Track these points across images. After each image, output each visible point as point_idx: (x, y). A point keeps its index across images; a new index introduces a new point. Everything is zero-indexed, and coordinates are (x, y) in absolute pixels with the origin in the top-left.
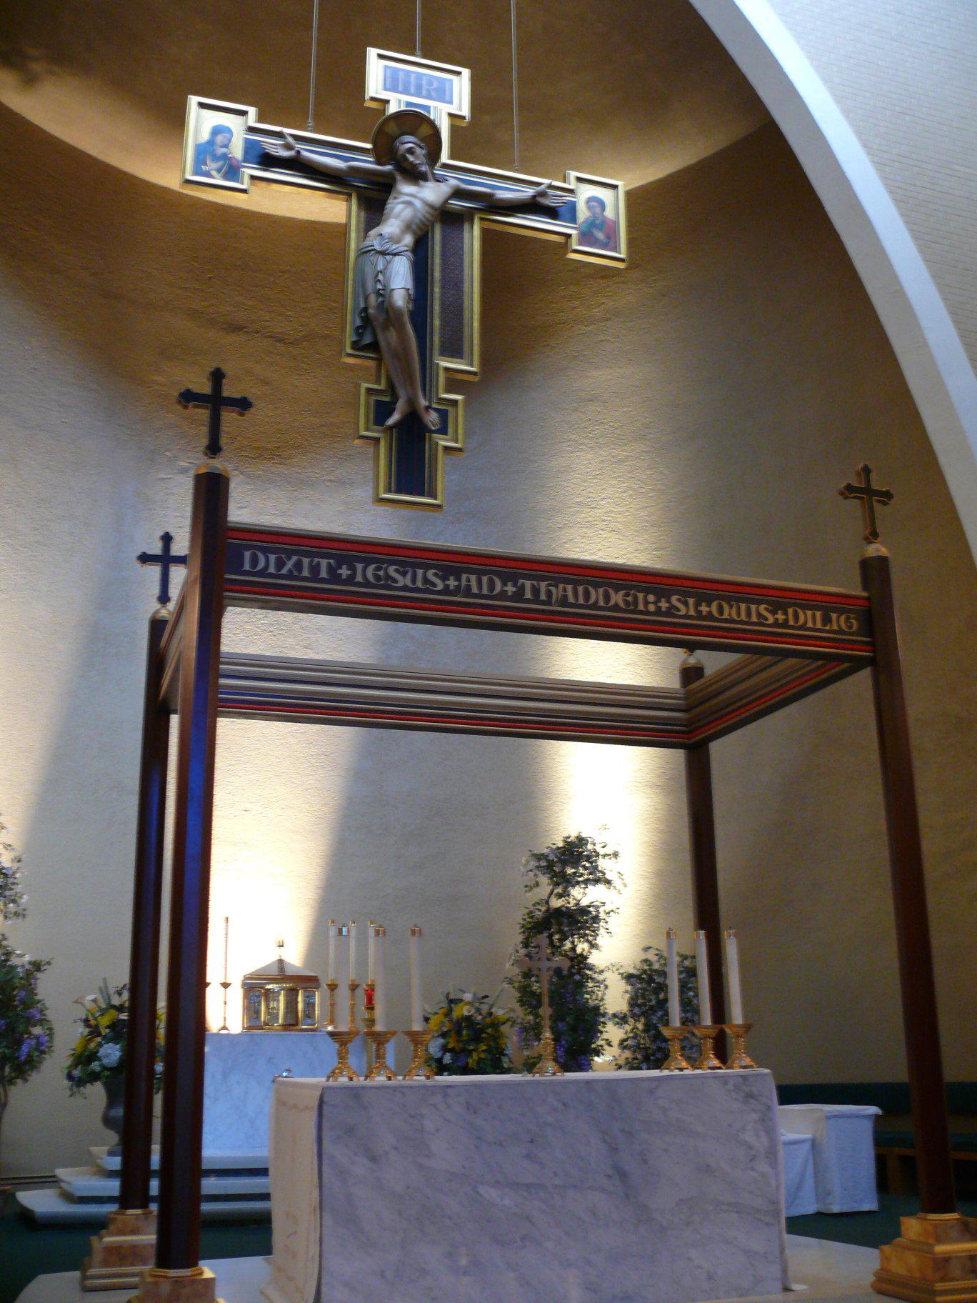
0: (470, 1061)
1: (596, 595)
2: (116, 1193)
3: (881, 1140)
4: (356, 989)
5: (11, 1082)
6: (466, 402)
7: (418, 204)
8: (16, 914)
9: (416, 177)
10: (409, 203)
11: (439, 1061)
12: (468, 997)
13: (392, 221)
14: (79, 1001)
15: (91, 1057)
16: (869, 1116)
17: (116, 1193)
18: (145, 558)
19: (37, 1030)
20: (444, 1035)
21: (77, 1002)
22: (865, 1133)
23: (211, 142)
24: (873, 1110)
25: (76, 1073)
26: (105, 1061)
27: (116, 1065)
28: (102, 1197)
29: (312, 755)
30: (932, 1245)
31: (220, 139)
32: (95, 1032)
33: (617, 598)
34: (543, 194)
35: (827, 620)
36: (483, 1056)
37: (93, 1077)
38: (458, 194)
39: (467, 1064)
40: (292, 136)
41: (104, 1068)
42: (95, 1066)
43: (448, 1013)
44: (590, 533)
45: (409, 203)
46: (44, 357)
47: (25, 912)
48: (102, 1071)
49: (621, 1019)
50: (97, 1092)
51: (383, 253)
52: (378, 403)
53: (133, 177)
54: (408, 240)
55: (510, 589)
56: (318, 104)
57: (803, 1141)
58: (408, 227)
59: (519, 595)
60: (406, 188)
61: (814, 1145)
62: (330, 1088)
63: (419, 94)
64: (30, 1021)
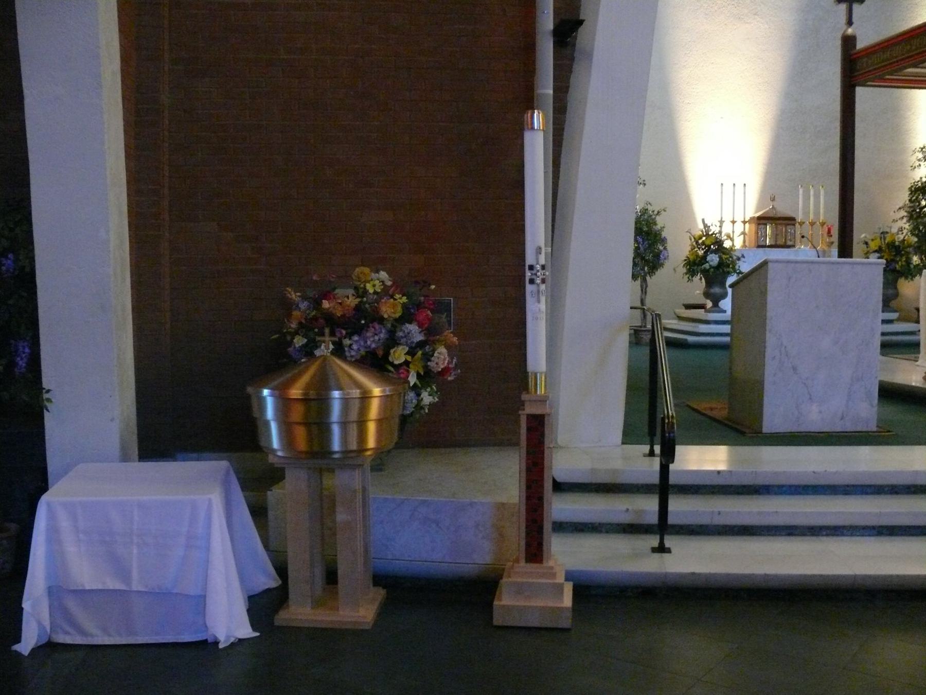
0: (897, 267)
2: (729, 331)
4: (814, 224)
14: (689, 231)
15: (704, 259)
17: (729, 331)
21: (687, 232)
26: (711, 263)
27: (716, 265)
28: (714, 333)
29: (760, 83)
36: (904, 263)
39: (896, 268)
41: (711, 267)
46: (333, 208)
47: (645, 182)
48: (710, 268)
49: (19, 361)
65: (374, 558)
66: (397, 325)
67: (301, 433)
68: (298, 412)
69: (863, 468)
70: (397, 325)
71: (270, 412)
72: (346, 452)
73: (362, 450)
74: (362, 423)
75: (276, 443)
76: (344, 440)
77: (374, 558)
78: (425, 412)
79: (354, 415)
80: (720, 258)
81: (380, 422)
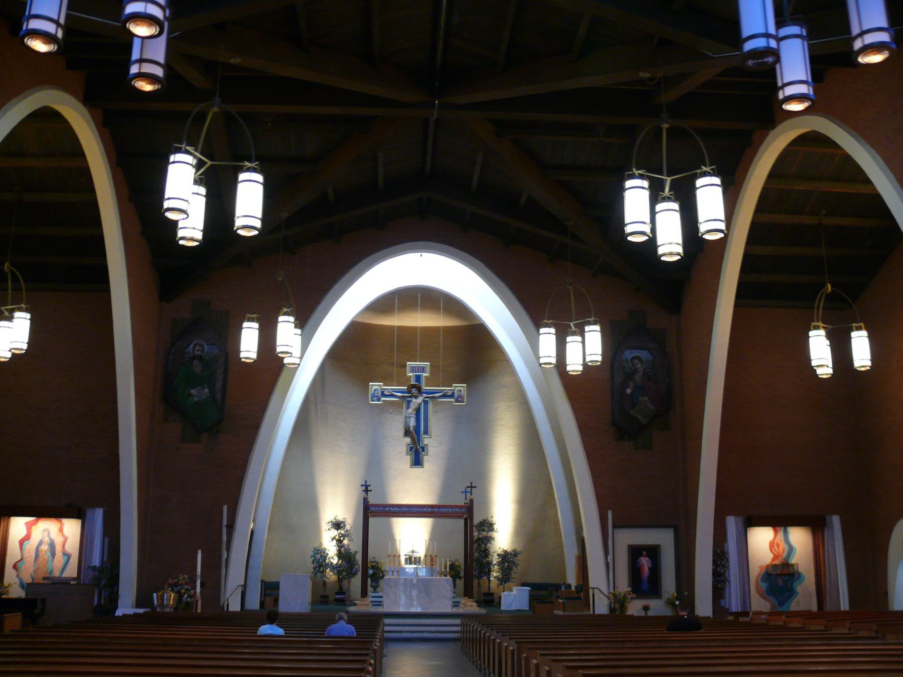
1: (422, 509)
3: (530, 596)
5: (352, 578)
6: (467, 386)
8: (351, 540)
9: (416, 397)
10: (414, 404)
13: (411, 408)
16: (528, 590)
19: (356, 566)
22: (707, 615)
24: (529, 588)
30: (333, 567)
31: (376, 392)
34: (446, 393)
35: (461, 510)
38: (426, 397)
40: (391, 389)
44: (503, 428)
45: (414, 404)
51: (409, 417)
52: (410, 447)
53: (372, 324)
54: (415, 412)
55: (408, 509)
56: (421, 303)
59: (410, 510)
60: (414, 400)
63: (418, 372)
65: (466, 499)
66: (495, 560)
67: (160, 601)
68: (159, 597)
69: (763, 159)
70: (495, 560)
71: (155, 597)
72: (167, 604)
73: (169, 604)
74: (170, 600)
75: (155, 602)
76: (167, 602)
77: (466, 499)
78: (342, 561)
79: (168, 598)
80: (374, 571)
81: (173, 600)
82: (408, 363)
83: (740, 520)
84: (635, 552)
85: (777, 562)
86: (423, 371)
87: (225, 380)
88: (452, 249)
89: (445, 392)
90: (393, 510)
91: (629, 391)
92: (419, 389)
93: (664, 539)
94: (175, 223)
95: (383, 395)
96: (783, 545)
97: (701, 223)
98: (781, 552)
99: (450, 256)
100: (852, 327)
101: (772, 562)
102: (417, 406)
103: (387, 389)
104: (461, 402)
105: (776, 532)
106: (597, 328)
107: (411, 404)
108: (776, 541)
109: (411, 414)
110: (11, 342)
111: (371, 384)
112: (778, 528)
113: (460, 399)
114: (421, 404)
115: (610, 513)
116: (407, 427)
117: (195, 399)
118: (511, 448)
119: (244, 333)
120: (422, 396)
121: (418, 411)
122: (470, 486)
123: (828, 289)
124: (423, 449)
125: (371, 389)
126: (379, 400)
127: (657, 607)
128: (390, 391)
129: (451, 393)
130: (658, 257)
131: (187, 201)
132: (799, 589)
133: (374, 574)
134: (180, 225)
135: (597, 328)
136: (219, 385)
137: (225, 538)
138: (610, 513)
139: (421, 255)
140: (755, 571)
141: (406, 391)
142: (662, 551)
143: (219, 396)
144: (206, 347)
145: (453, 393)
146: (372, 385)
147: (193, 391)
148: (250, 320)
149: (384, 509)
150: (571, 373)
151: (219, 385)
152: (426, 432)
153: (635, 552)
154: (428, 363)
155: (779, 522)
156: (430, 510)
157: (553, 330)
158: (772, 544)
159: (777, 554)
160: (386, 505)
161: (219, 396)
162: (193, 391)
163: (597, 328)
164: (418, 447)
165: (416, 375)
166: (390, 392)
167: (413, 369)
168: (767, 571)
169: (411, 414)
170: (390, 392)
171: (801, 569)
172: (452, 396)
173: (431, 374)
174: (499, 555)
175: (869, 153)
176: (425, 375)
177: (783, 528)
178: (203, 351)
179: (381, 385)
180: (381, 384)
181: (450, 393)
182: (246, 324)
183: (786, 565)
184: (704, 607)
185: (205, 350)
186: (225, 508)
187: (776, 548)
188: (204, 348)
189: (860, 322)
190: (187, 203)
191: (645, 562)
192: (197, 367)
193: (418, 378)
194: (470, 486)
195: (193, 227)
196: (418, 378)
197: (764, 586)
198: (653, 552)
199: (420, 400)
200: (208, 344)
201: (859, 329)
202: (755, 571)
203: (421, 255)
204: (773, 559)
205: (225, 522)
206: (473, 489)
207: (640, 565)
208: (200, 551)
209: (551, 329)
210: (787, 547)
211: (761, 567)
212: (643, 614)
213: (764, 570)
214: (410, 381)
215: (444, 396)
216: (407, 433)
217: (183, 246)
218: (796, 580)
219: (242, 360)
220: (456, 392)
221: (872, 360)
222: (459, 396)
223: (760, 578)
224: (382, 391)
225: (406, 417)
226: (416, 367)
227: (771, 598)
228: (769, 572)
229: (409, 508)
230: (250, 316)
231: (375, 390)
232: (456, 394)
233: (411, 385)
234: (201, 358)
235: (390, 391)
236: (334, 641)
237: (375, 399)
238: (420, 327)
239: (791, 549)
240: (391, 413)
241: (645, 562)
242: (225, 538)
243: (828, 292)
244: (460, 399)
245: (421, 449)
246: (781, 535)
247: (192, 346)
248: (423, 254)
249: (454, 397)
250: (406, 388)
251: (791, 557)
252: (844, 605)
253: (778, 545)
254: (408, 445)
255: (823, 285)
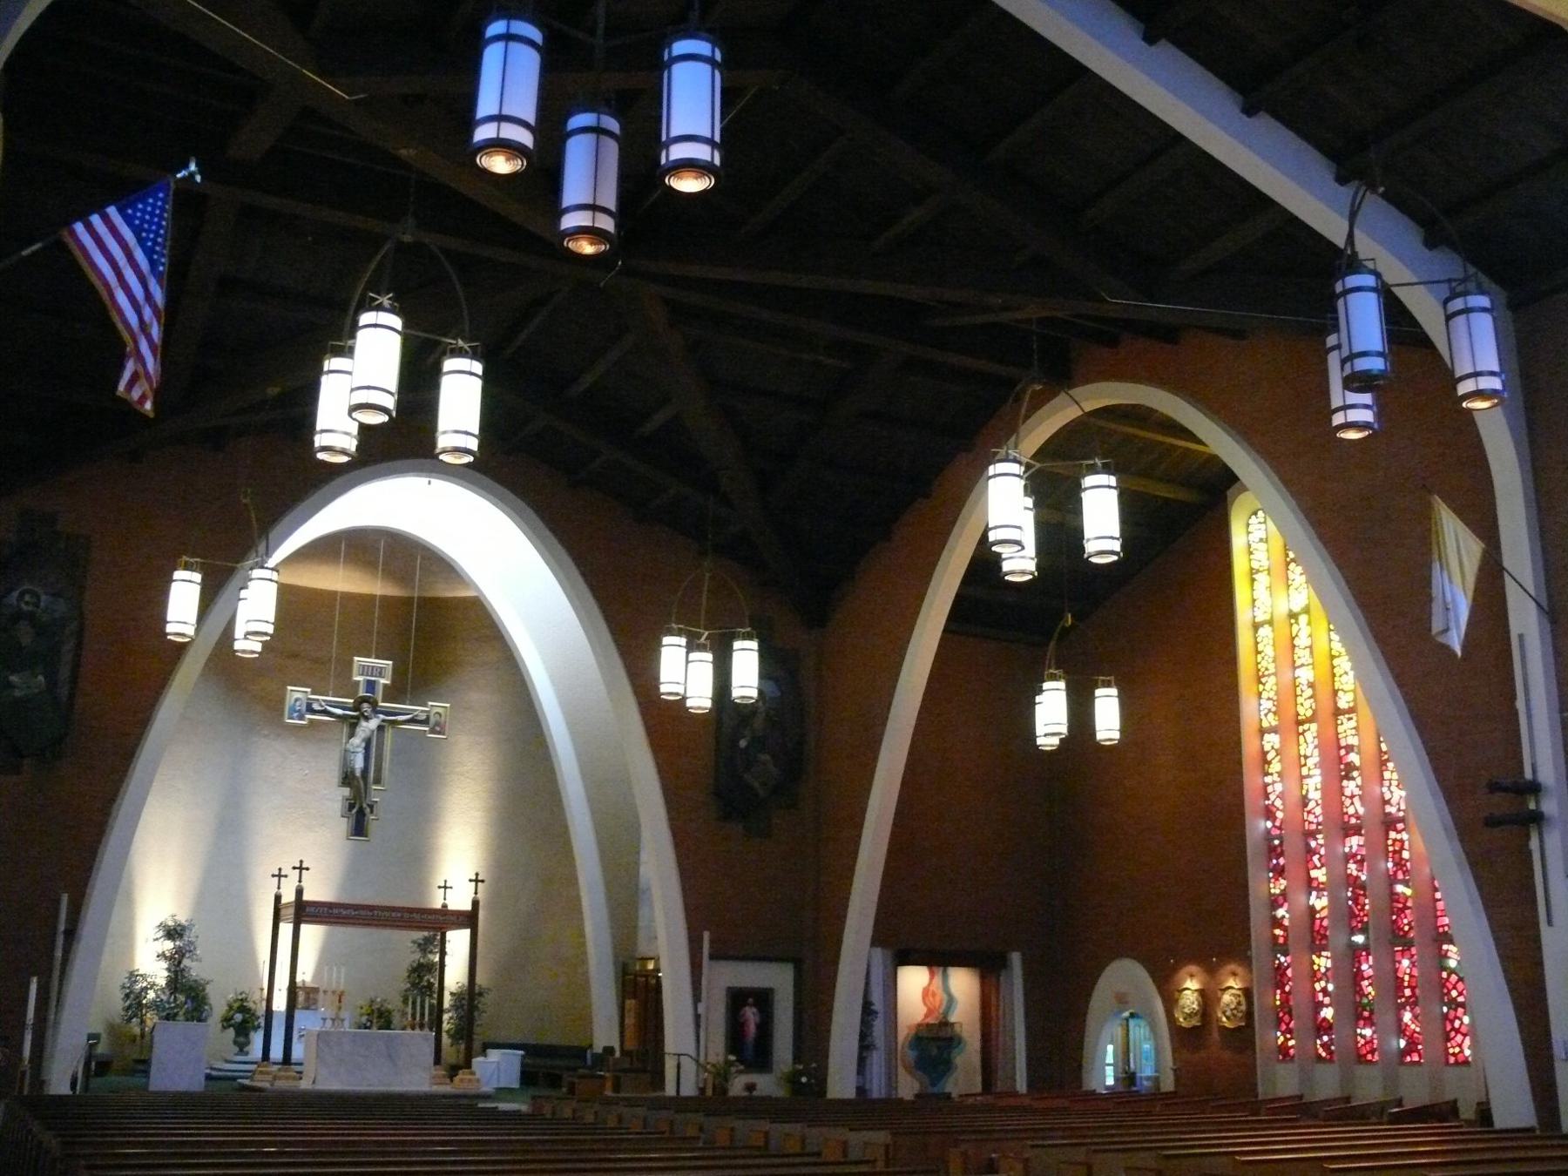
1: (394, 914)
3: (523, 1065)
7: (367, 730)
8: (197, 960)
9: (367, 719)
11: (365, 1024)
12: (379, 1000)
16: (518, 1055)
18: (273, 876)
19: (206, 1007)
20: (369, 1015)
23: (294, 705)
24: (521, 1052)
25: (225, 1024)
31: (298, 703)
32: (230, 1007)
33: (399, 915)
34: (416, 716)
37: (230, 1026)
38: (383, 721)
40: (324, 701)
42: (233, 1021)
43: (370, 1006)
44: (462, 778)
50: (231, 1032)
54: (363, 745)
57: (494, 1062)
58: (363, 740)
60: (364, 723)
61: (498, 1063)
62: (323, 1032)
63: (372, 676)
64: (206, 1004)
80: (244, 1016)
82: (356, 659)
83: (889, 953)
84: (737, 998)
85: (931, 1021)
86: (381, 675)
87: (76, 665)
88: (398, 463)
89: (416, 713)
90: (344, 913)
91: (743, 743)
92: (374, 704)
93: (778, 978)
94: (999, 555)
95: (311, 710)
96: (941, 995)
97: (1088, 540)
98: (937, 1005)
99: (471, 486)
100: (1097, 681)
101: (923, 1020)
102: (368, 733)
103: (318, 700)
104: (439, 733)
105: (932, 975)
106: (754, 645)
107: (358, 730)
108: (931, 988)
109: (358, 747)
110: (249, 621)
111: (289, 688)
112: (935, 969)
113: (438, 729)
114: (373, 731)
115: (706, 935)
116: (349, 770)
117: (17, 693)
118: (478, 814)
119: (175, 589)
120: (378, 717)
121: (368, 742)
122: (304, 871)
123: (1067, 621)
124: (371, 807)
125: (291, 697)
126: (301, 717)
127: (767, 1085)
128: (323, 704)
129: (425, 717)
130: (1001, 575)
131: (1019, 528)
132: (959, 1060)
133: (244, 1021)
134: (1004, 556)
135: (1114, 691)
136: (64, 673)
137: (59, 954)
138: (706, 935)
139: (429, 483)
140: (903, 1033)
141: (351, 706)
142: (777, 998)
143: (64, 692)
144: (43, 598)
145: (428, 718)
146: (292, 690)
147: (14, 678)
148: (187, 567)
149: (330, 911)
150: (239, 654)
151: (64, 673)
152: (378, 781)
153: (737, 998)
154: (390, 662)
155: (938, 959)
156: (406, 915)
157: (197, 577)
158: (926, 993)
159: (931, 1007)
160: (424, 909)
161: (64, 692)
162: (14, 678)
163: (754, 645)
164: (365, 805)
165: (368, 681)
166: (322, 706)
167: (365, 670)
168: (916, 1034)
169: (358, 747)
170: (322, 706)
171: (965, 1035)
172: (425, 722)
173: (393, 681)
174: (452, 994)
175: (1259, 466)
176: (383, 681)
177: (941, 969)
178: (37, 605)
179: (306, 692)
180: (309, 690)
181: (423, 717)
182: (666, 640)
183: (945, 1024)
184: (841, 1084)
185: (42, 604)
186: (65, 898)
187: (931, 999)
188: (39, 600)
189: (1110, 675)
190: (1019, 530)
191: (751, 1015)
192: (25, 635)
193: (371, 686)
194: (277, 873)
195: (344, 430)
196: (371, 686)
197: (911, 1055)
198: (763, 999)
199: (373, 724)
200: (46, 594)
201: (1107, 685)
202: (903, 1033)
203: (429, 483)
204: (926, 1016)
205: (62, 927)
206: (282, 879)
207: (742, 1020)
208: (35, 980)
209: (194, 574)
210: (945, 997)
211: (909, 1027)
212: (746, 1094)
213: (913, 1032)
214: (357, 691)
215: (413, 721)
216: (347, 779)
217: (323, 462)
218: (955, 1047)
219: (169, 637)
220: (432, 714)
221: (1122, 731)
222: (437, 724)
223: (907, 1043)
224: (308, 703)
225: (346, 751)
226: (368, 666)
227: (919, 1073)
228: (920, 1035)
229: (371, 911)
230: (188, 559)
231: (297, 700)
232: (432, 720)
233: (361, 697)
234: (31, 617)
235: (323, 704)
236: (239, 1141)
237: (296, 715)
238: (342, 593)
239: (951, 1000)
240: (265, 736)
241: (751, 1015)
242: (59, 954)
243: (1067, 625)
244: (438, 729)
245: (368, 810)
246: (938, 980)
247: (15, 594)
248: (432, 480)
249: (428, 723)
250: (352, 701)
251: (950, 1013)
252: (1022, 1086)
253: (934, 995)
254: (347, 800)
255: (1061, 617)
